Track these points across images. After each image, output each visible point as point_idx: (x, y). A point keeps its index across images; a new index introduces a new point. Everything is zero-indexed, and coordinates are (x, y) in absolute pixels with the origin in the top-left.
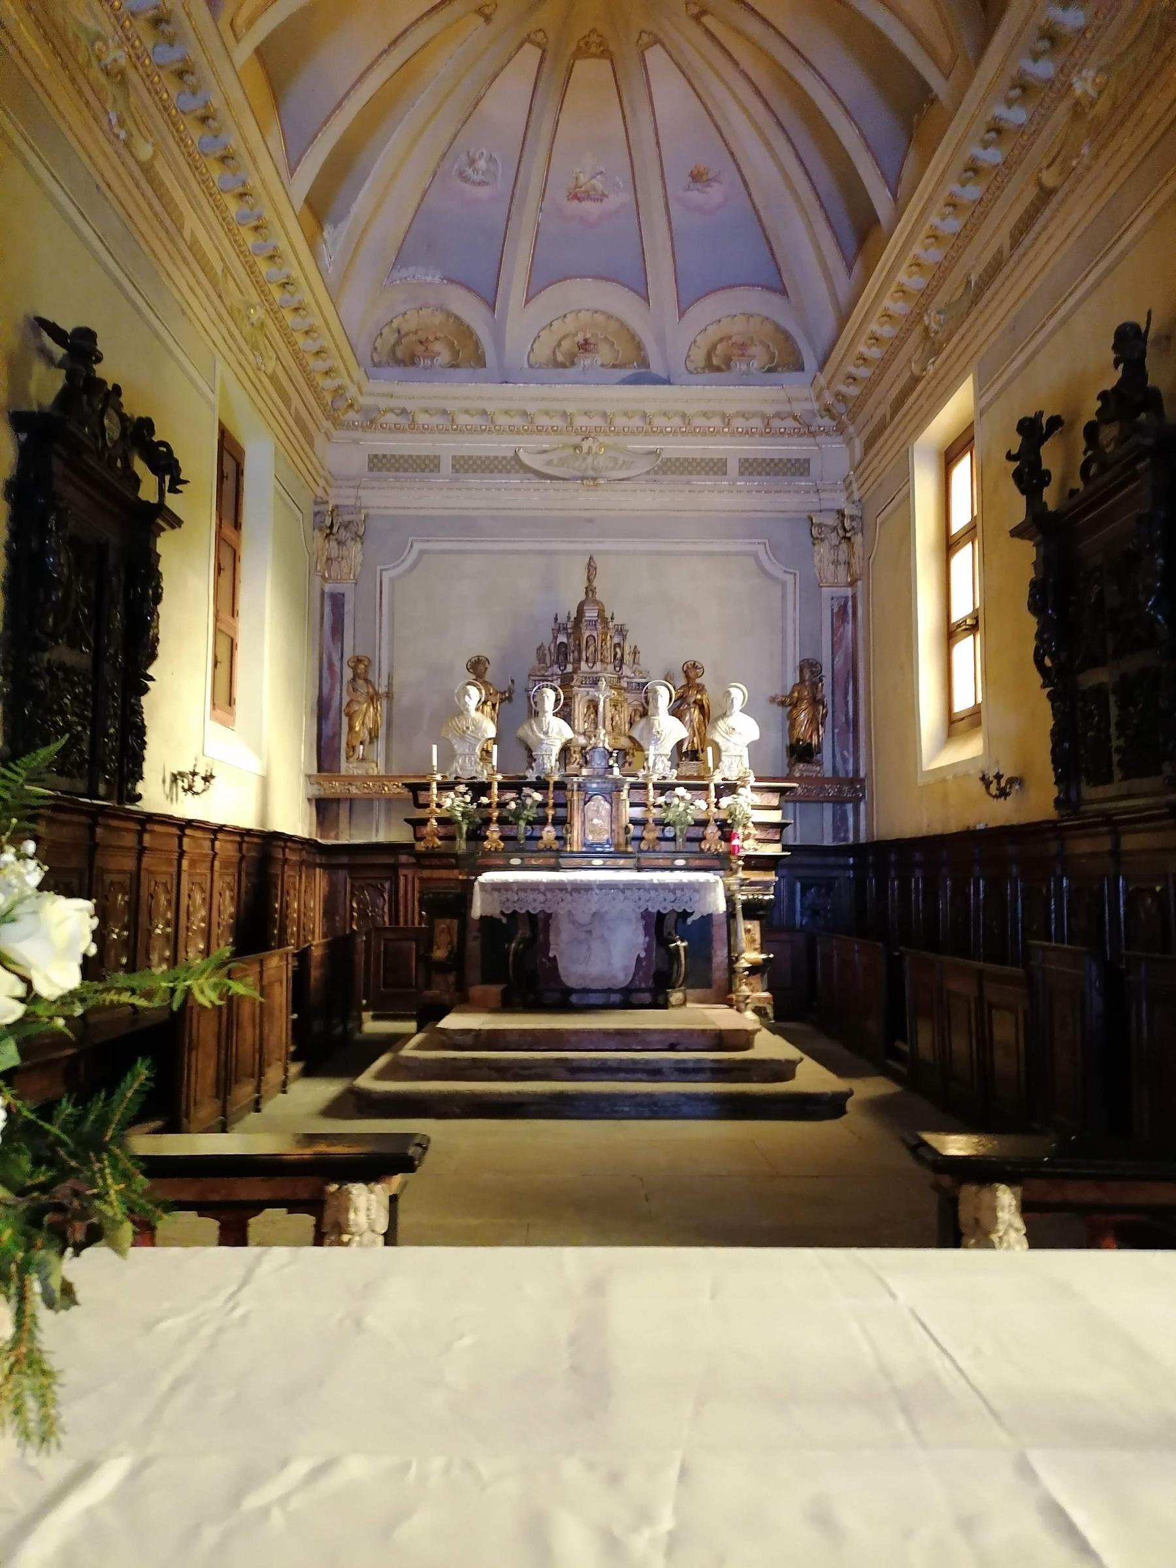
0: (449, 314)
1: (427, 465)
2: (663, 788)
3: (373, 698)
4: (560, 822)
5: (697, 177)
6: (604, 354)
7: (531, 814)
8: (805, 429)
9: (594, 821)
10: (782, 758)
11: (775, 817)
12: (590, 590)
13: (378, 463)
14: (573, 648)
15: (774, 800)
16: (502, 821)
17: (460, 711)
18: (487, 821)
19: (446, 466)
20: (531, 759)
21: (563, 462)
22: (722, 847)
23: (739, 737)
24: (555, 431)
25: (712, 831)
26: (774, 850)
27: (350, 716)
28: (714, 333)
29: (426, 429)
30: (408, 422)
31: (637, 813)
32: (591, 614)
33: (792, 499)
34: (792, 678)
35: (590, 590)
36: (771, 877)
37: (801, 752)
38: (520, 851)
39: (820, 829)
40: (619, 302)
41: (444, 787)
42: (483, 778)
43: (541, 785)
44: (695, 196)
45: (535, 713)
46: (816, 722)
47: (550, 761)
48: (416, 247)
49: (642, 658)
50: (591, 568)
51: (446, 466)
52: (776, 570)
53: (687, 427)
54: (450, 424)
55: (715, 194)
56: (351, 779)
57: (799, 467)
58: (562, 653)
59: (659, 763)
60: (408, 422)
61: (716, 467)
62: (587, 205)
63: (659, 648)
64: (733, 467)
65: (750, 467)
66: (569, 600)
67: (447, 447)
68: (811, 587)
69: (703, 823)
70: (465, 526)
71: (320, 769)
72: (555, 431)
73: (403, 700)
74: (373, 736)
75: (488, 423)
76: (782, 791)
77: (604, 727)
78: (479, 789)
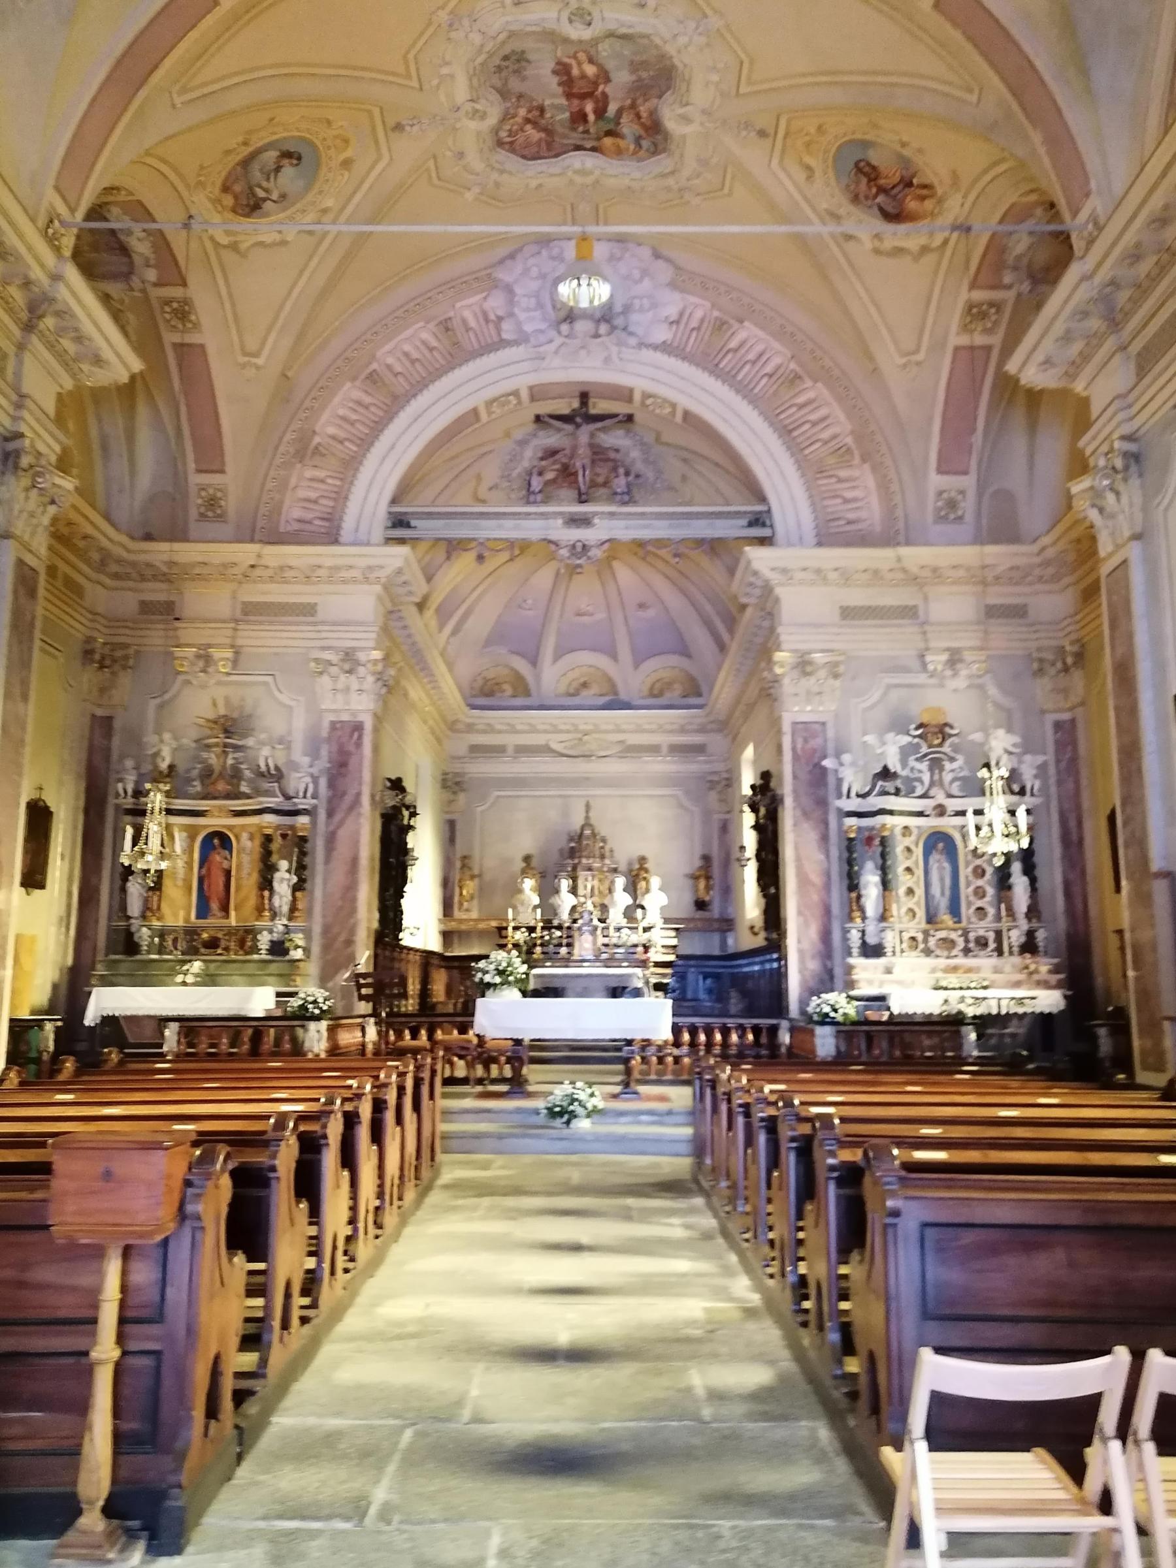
0: (512, 669)
1: (500, 750)
2: (618, 929)
3: (472, 877)
4: (569, 945)
5: (642, 606)
6: (595, 689)
7: (555, 942)
8: (702, 730)
9: (584, 945)
10: (692, 907)
11: (674, 942)
12: (587, 818)
13: (475, 749)
14: (574, 853)
15: (673, 934)
16: (542, 945)
17: (520, 891)
18: (535, 945)
19: (510, 750)
20: (556, 914)
21: (572, 748)
22: (644, 957)
23: (656, 900)
24: (568, 732)
25: (640, 949)
26: (672, 958)
27: (461, 888)
28: (655, 677)
29: (500, 732)
30: (490, 729)
31: (606, 940)
32: (587, 832)
33: (695, 766)
34: (698, 863)
35: (587, 818)
36: (669, 971)
37: (701, 905)
38: (550, 959)
39: (696, 946)
40: (602, 661)
41: (516, 928)
42: (532, 924)
43: (559, 928)
44: (641, 613)
45: (557, 891)
46: (708, 888)
47: (565, 916)
48: (497, 637)
49: (616, 854)
50: (588, 807)
51: (510, 750)
52: (687, 803)
53: (640, 730)
54: (513, 730)
55: (651, 613)
56: (461, 921)
57: (699, 749)
58: (573, 853)
59: (616, 916)
60: (490, 729)
61: (654, 749)
62: (585, 619)
63: (625, 849)
64: (665, 750)
65: (675, 749)
66: (577, 821)
67: (511, 740)
68: (707, 815)
69: (636, 946)
70: (519, 782)
71: (445, 915)
72: (568, 732)
73: (488, 877)
74: (472, 898)
75: (533, 730)
76: (677, 930)
77: (965, 197)
78: (531, 930)
